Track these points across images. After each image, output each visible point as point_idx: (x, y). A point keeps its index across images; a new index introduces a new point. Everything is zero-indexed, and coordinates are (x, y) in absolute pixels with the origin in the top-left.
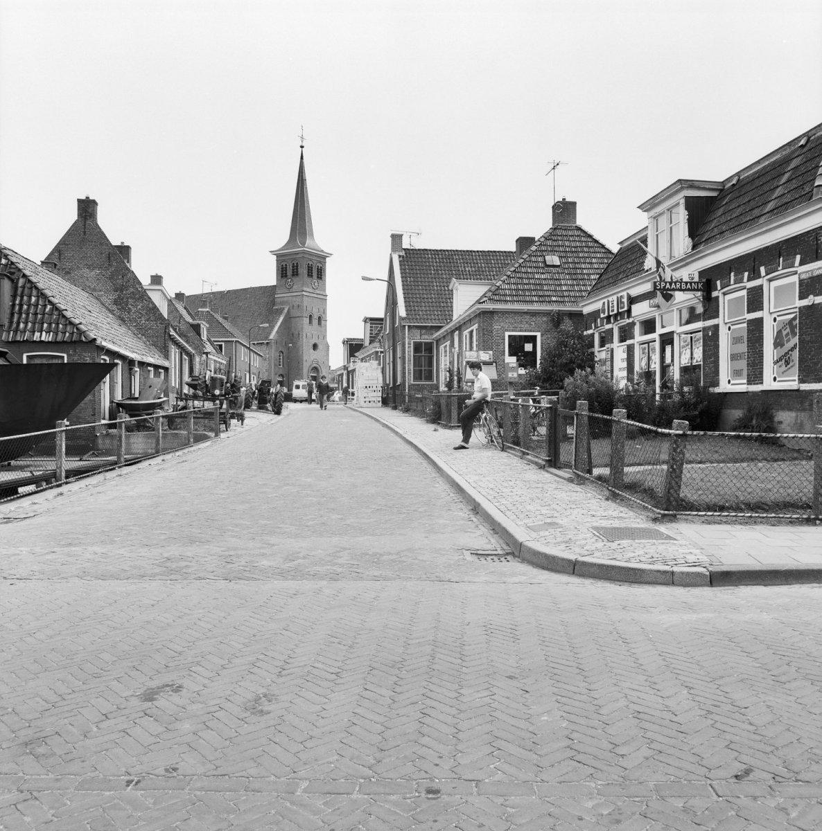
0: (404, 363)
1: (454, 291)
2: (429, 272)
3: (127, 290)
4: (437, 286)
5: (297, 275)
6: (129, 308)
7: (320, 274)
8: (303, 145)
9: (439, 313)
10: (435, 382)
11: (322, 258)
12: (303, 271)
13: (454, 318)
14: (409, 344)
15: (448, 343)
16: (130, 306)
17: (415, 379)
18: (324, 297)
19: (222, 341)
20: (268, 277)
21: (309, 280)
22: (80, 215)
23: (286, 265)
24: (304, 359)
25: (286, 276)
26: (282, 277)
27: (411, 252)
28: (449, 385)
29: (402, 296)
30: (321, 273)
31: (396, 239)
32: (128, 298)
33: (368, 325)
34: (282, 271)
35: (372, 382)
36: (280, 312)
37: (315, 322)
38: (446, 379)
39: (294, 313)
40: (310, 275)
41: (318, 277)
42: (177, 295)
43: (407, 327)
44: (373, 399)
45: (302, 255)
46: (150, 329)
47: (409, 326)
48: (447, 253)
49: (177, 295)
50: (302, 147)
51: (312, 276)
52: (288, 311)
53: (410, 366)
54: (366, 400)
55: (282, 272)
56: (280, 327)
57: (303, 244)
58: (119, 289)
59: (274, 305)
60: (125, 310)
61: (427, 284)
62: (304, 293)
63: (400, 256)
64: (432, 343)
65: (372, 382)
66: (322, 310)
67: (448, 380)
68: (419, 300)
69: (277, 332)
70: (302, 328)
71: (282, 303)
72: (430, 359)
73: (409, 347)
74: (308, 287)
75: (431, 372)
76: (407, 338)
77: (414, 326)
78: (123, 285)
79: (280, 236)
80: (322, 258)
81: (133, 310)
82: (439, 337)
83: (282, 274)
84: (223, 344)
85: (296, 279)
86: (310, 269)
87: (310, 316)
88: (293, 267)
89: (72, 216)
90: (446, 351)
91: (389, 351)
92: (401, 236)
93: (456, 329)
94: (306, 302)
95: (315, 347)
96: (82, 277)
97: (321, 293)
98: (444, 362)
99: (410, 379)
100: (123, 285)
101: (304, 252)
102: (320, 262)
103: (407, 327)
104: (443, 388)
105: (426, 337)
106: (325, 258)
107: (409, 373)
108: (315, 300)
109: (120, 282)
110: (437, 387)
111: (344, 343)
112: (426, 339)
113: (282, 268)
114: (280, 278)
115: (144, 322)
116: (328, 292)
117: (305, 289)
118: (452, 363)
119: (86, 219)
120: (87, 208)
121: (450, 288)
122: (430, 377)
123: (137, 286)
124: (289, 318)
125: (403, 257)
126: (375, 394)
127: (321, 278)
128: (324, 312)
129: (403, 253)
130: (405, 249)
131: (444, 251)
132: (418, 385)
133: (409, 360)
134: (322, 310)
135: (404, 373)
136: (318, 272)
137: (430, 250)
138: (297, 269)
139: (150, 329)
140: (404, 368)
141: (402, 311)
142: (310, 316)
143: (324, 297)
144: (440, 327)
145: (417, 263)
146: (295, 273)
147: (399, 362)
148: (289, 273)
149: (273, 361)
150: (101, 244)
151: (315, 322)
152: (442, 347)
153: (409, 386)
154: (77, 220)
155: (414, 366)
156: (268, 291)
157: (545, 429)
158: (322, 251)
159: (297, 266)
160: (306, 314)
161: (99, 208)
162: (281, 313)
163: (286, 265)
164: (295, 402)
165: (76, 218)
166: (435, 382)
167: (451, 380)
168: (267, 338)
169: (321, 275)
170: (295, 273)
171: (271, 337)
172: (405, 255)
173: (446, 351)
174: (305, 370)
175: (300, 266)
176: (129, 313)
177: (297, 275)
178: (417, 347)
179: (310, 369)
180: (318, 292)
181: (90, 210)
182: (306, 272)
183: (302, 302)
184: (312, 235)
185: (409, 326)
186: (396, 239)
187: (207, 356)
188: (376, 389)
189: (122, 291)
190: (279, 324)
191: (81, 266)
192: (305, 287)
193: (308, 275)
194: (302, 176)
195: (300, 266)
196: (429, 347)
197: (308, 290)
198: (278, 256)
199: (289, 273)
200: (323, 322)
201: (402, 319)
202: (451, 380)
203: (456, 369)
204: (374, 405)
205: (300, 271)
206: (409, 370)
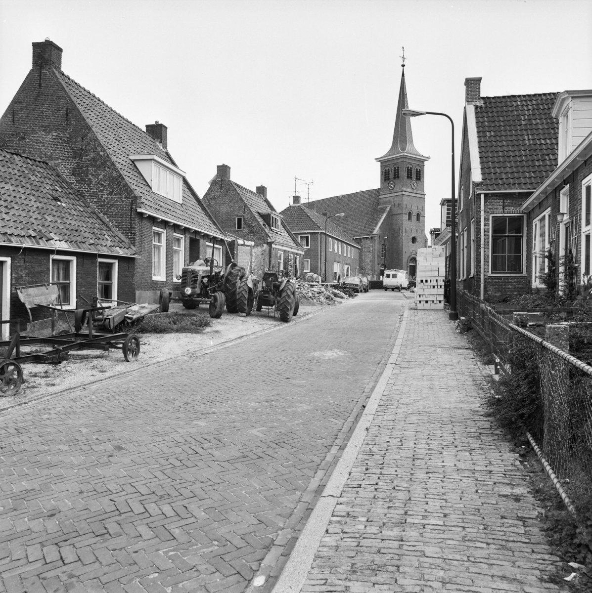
0: (478, 247)
1: (561, 120)
2: (518, 123)
3: (87, 156)
4: (529, 140)
5: (398, 177)
6: (89, 179)
7: (419, 176)
8: (404, 63)
9: (532, 174)
10: (525, 274)
11: (421, 161)
12: (403, 174)
13: (560, 162)
14: (486, 220)
15: (547, 212)
16: (90, 176)
17: (494, 269)
18: (423, 196)
19: (308, 233)
20: (373, 181)
21: (408, 181)
22: (35, 63)
23: (389, 170)
24: (404, 251)
25: (389, 179)
26: (385, 180)
27: (493, 101)
28: (550, 280)
29: (478, 155)
30: (420, 174)
31: (473, 84)
32: (87, 166)
33: (445, 207)
34: (385, 175)
35: (430, 274)
36: (383, 211)
37: (414, 218)
38: (542, 269)
39: (396, 211)
40: (409, 177)
41: (417, 179)
42: (258, 188)
43: (482, 196)
44: (432, 298)
45: (402, 160)
46: (113, 205)
47: (486, 195)
48: (544, 97)
49: (258, 188)
50: (403, 66)
51: (411, 178)
52: (391, 209)
53: (486, 252)
54: (421, 299)
55: (386, 176)
56: (382, 223)
57: (404, 150)
58: (78, 155)
59: (378, 205)
60: (85, 182)
61: (514, 138)
62: (404, 193)
63: (476, 107)
64: (520, 218)
65: (430, 274)
66: (420, 207)
67: (546, 271)
68: (502, 160)
69: (380, 228)
70: (402, 224)
71: (385, 203)
72: (519, 240)
73: (485, 225)
74: (408, 188)
75: (518, 259)
76: (482, 213)
77: (492, 194)
78: (82, 150)
79: (384, 145)
80: (421, 161)
81: (94, 181)
82: (531, 207)
83: (385, 178)
84: (309, 235)
85: (397, 181)
86: (409, 172)
87: (410, 213)
88: (394, 171)
89: (25, 65)
90: (543, 227)
91: (463, 234)
92: (480, 80)
93: (565, 182)
94: (406, 200)
95: (414, 240)
96: (38, 142)
97: (420, 192)
98: (539, 245)
99: (487, 271)
100: (82, 150)
101: (404, 157)
102: (419, 165)
103: (482, 196)
104: (536, 284)
105: (512, 209)
106: (423, 161)
107: (486, 261)
108: (414, 198)
109: (78, 145)
110: (528, 280)
111: (431, 234)
112: (512, 212)
113: (385, 173)
114: (383, 181)
115: (106, 196)
116: (426, 192)
117: (404, 189)
118: (554, 243)
119: (41, 67)
120: (46, 54)
121: (553, 115)
122: (516, 265)
123: (99, 149)
124: (391, 215)
125: (481, 107)
126: (434, 291)
127: (420, 179)
128: (423, 209)
129: (481, 103)
130: (483, 98)
131: (540, 95)
132: (499, 278)
133: (486, 244)
134: (420, 207)
135: (478, 261)
136: (417, 174)
137: (519, 96)
138: (398, 172)
139: (113, 205)
140: (478, 255)
141: (477, 176)
142: (410, 213)
143: (423, 196)
144: (530, 194)
145: (500, 113)
146: (397, 176)
147: (473, 245)
148: (391, 176)
149: (376, 253)
150: (58, 98)
151: (414, 218)
152: (536, 221)
153: (485, 279)
154: (32, 70)
155: (493, 252)
156: (374, 194)
157: (560, 277)
158: (422, 156)
159: (398, 170)
160: (406, 211)
161: (64, 55)
162: (384, 211)
163: (389, 170)
164: (386, 290)
165: (30, 67)
166: (525, 274)
167: (553, 272)
168: (371, 233)
169: (420, 177)
170: (397, 176)
171: (374, 232)
172: (483, 105)
173: (543, 227)
174: (404, 261)
175: (402, 170)
176: (89, 185)
177: (398, 177)
178: (499, 226)
179: (410, 258)
180: (417, 192)
181: (46, 56)
182: (405, 174)
183: (402, 201)
184: (412, 142)
185: (486, 195)
186: (473, 84)
187: (271, 246)
188: (435, 284)
189: (81, 157)
190: (382, 220)
191: (37, 128)
192: (406, 188)
193: (408, 177)
194: (403, 90)
195: (402, 170)
196: (516, 223)
197: (408, 190)
198: (382, 162)
199: (391, 176)
200: (421, 218)
201: (477, 185)
202: (553, 272)
203: (562, 253)
204: (433, 306)
205: (401, 173)
206: (486, 256)
